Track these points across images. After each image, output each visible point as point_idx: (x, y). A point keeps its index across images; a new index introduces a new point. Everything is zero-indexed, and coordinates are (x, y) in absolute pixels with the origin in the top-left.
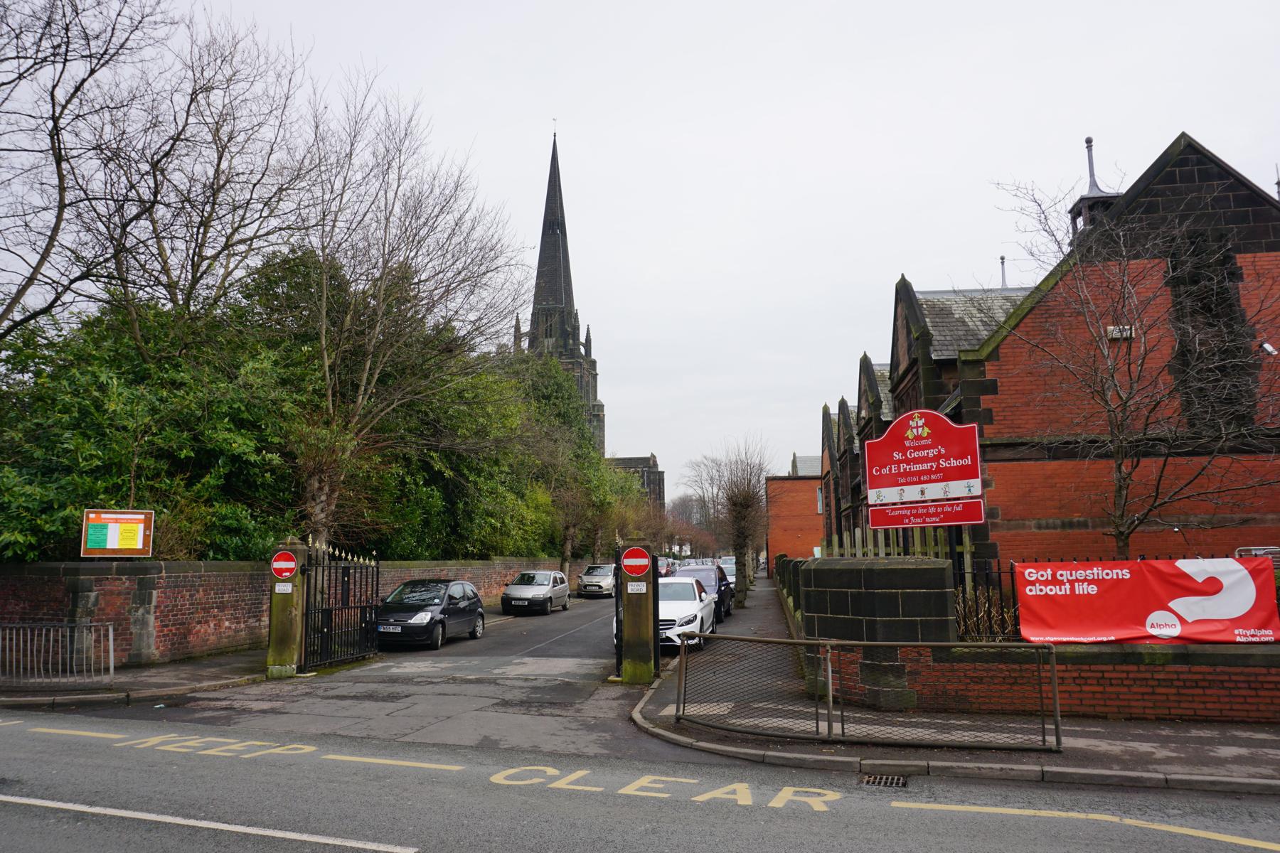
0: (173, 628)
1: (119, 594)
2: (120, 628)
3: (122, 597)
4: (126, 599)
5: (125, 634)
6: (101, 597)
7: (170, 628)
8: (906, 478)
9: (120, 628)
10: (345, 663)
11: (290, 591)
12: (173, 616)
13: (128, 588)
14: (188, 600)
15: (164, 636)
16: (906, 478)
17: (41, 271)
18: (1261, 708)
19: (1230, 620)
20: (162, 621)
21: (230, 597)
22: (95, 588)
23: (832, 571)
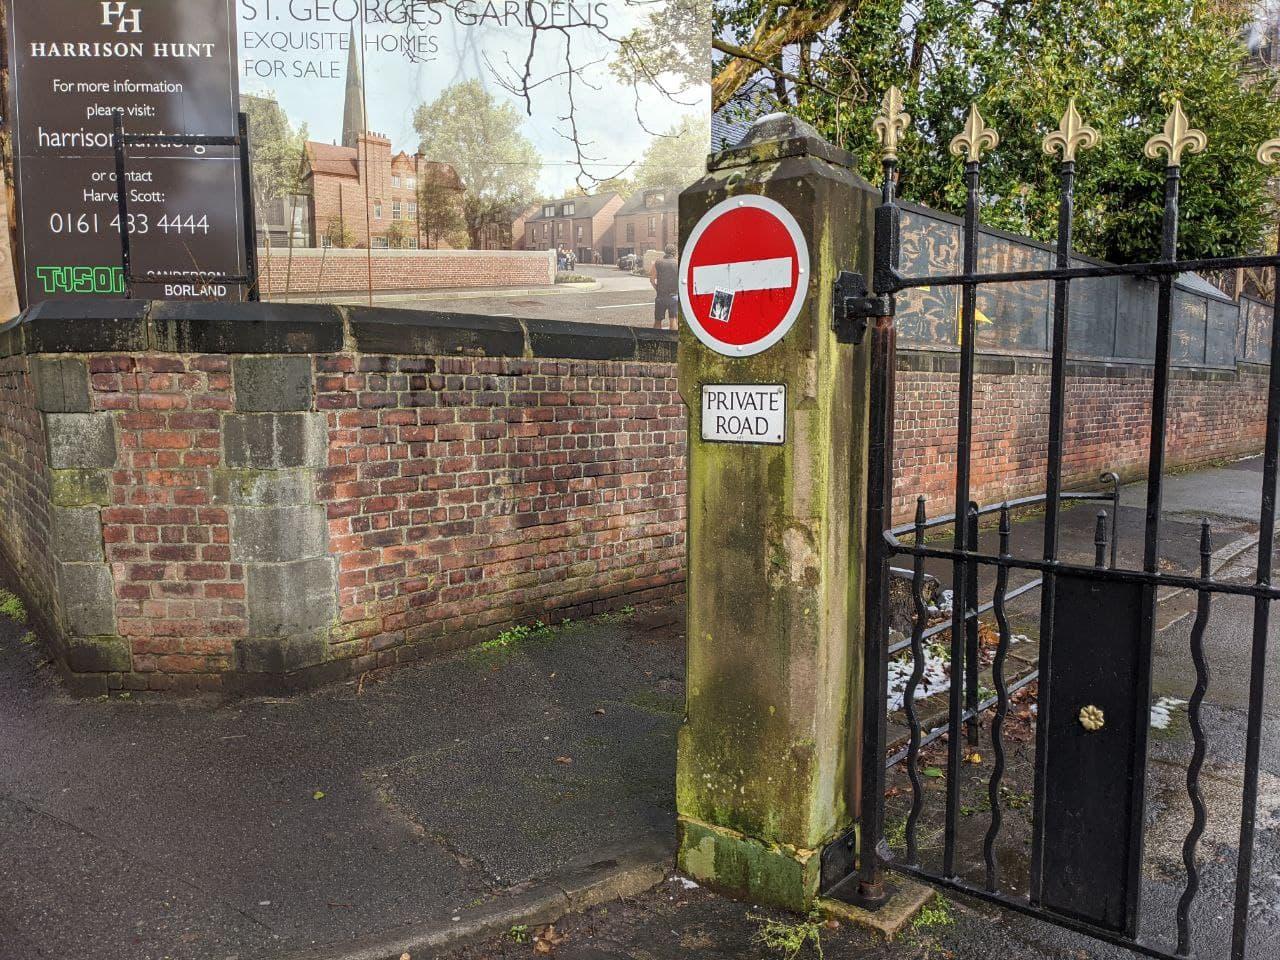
0: (418, 546)
1: (179, 422)
2: (199, 547)
3: (194, 434)
4: (205, 439)
5: (218, 573)
6: (119, 431)
7: (405, 545)
8: (287, 298)
9: (199, 547)
10: (1062, 325)
11: (774, 432)
12: (411, 503)
13: (204, 400)
14: (474, 449)
15: (377, 574)
16: (287, 298)
17: (898, 347)
18: (1245, 571)
19: (811, 273)
20: (360, 525)
21: (634, 440)
22: (97, 397)
23: (1146, 729)
